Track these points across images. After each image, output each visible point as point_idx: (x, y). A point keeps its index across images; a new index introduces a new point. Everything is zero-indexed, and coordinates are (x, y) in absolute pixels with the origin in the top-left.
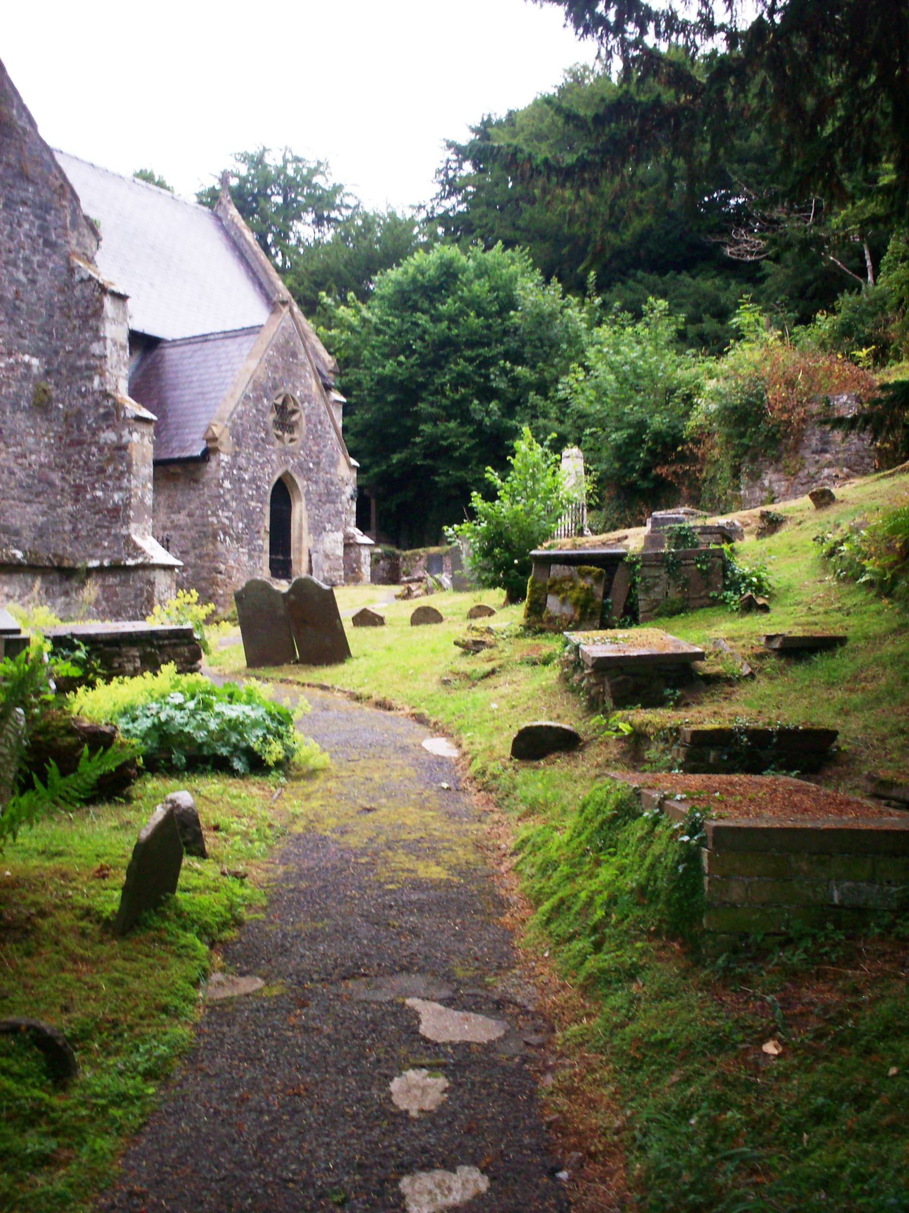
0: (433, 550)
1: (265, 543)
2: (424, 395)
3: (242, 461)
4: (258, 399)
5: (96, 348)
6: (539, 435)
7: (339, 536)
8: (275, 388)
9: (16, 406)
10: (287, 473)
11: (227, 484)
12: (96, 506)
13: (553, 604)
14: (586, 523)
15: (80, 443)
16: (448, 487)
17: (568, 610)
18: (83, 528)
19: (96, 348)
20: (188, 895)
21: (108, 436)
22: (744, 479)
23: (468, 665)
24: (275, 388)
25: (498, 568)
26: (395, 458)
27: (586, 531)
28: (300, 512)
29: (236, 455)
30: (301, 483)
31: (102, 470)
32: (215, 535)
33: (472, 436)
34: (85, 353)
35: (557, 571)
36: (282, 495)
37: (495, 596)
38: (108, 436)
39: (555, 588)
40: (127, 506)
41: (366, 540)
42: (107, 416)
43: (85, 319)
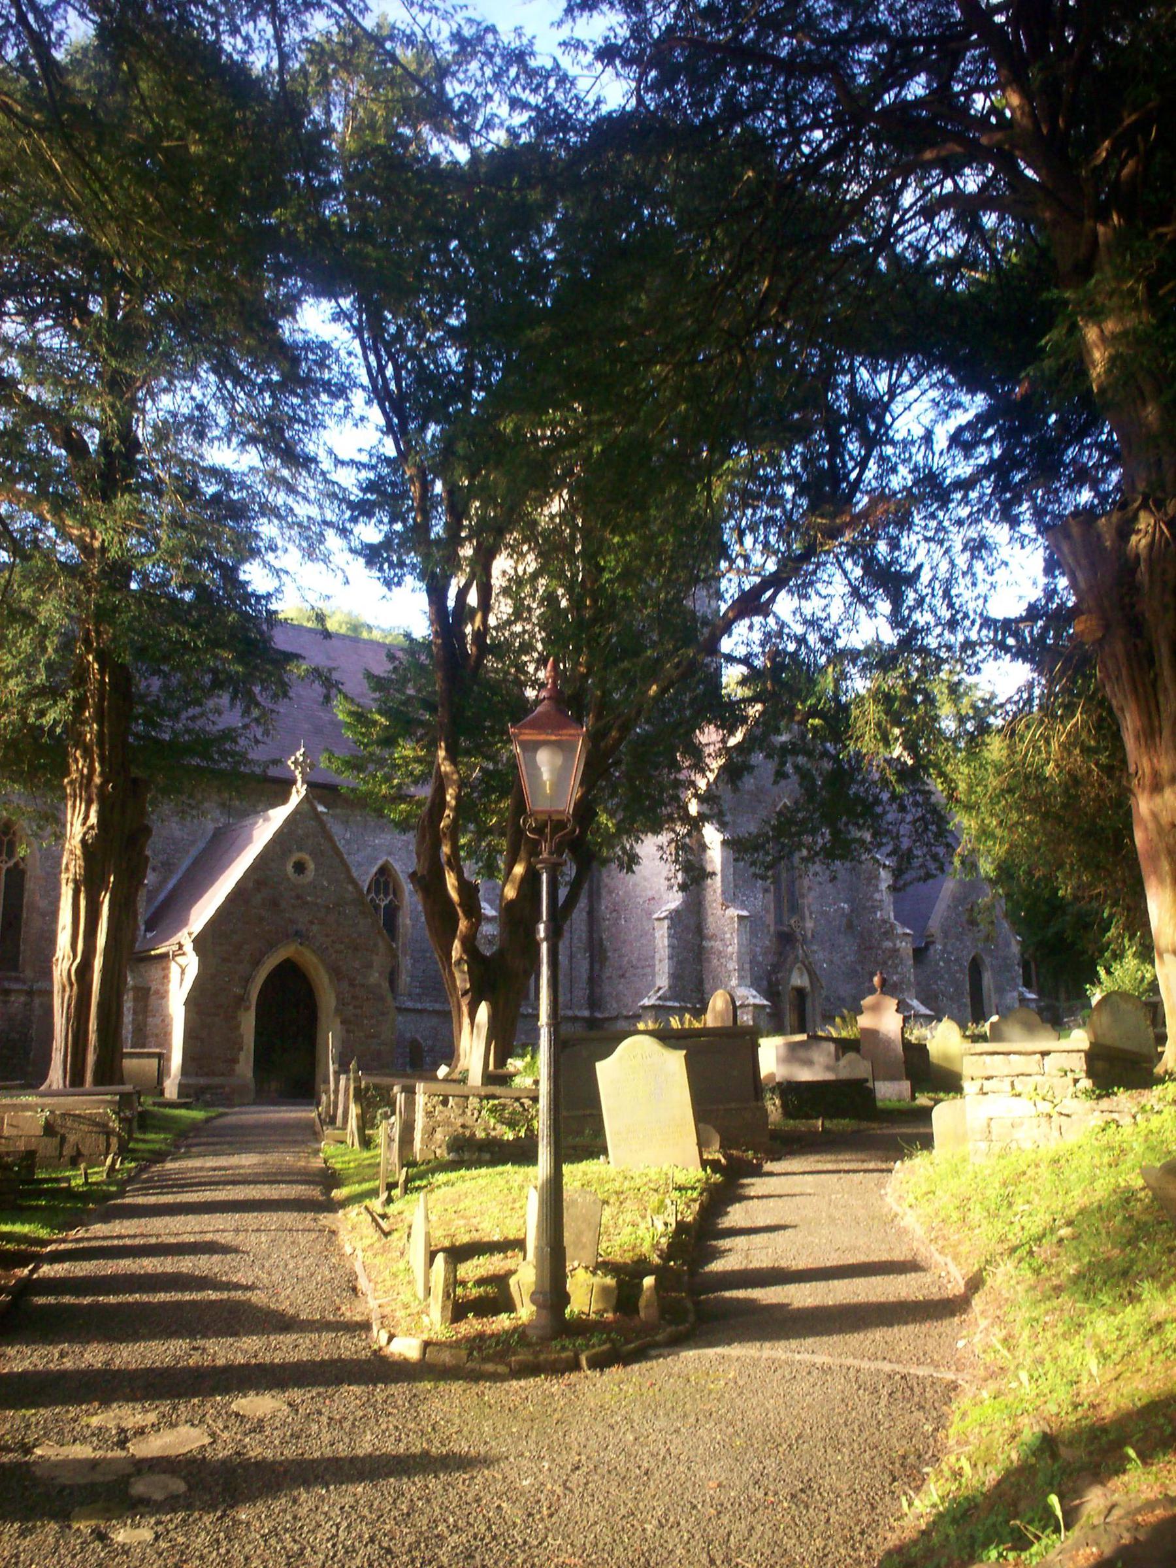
1: (967, 1000)
3: (949, 948)
4: (956, 907)
6: (606, 810)
7: (1015, 994)
8: (965, 898)
9: (839, 931)
10: (387, 862)
15: (871, 948)
20: (135, 1061)
21: (888, 944)
24: (965, 898)
28: (987, 979)
29: (945, 945)
30: (987, 960)
31: (885, 963)
32: (937, 997)
34: (871, 898)
36: (975, 969)
38: (888, 944)
41: (1033, 996)
42: (886, 933)
43: (869, 879)
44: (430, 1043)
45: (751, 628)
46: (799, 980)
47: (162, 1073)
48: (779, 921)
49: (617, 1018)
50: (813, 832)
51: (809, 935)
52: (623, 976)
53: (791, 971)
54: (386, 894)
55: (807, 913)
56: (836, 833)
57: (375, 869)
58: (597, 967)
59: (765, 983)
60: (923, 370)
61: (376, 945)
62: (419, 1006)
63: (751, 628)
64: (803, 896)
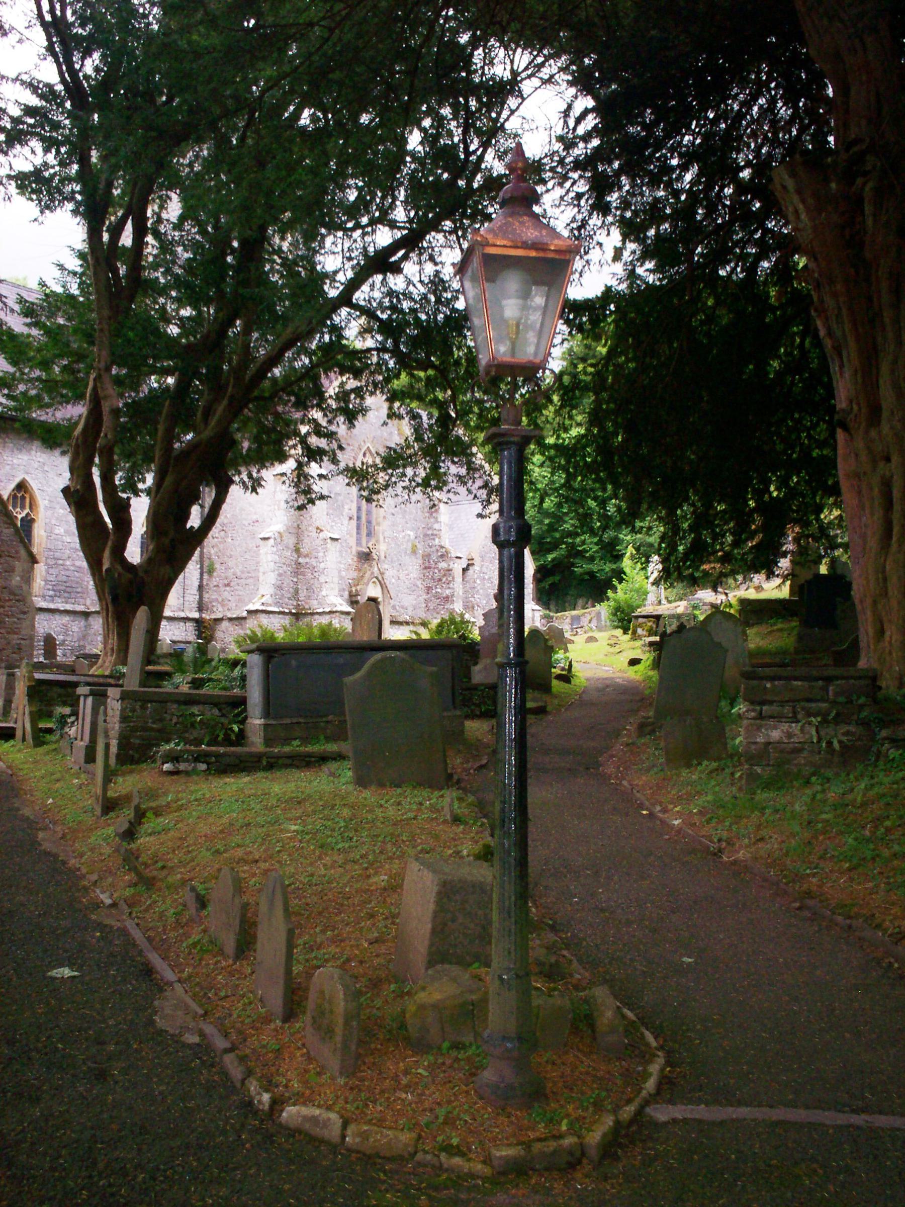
0: (574, 613)
2: (567, 519)
3: (484, 570)
5: (436, 526)
11: (478, 581)
12: (437, 596)
13: (639, 631)
14: (663, 597)
16: (581, 574)
17: (645, 633)
18: (431, 606)
19: (436, 526)
21: (443, 565)
22: (162, 801)
23: (612, 650)
25: (619, 621)
26: (550, 557)
27: (664, 601)
31: (440, 580)
33: (596, 544)
35: (640, 620)
37: (619, 632)
38: (443, 565)
39: (640, 626)
40: (453, 596)
42: (442, 556)
44: (61, 637)
45: (372, 286)
46: (373, 591)
47: (812, 737)
48: (359, 543)
49: (221, 620)
50: (415, 465)
51: (382, 557)
52: (228, 585)
53: (367, 584)
54: (23, 507)
55: (381, 538)
56: (435, 468)
57: (12, 486)
58: (206, 576)
59: (347, 593)
60: (556, 56)
61: (17, 552)
62: (52, 606)
63: (372, 286)
64: (378, 524)
